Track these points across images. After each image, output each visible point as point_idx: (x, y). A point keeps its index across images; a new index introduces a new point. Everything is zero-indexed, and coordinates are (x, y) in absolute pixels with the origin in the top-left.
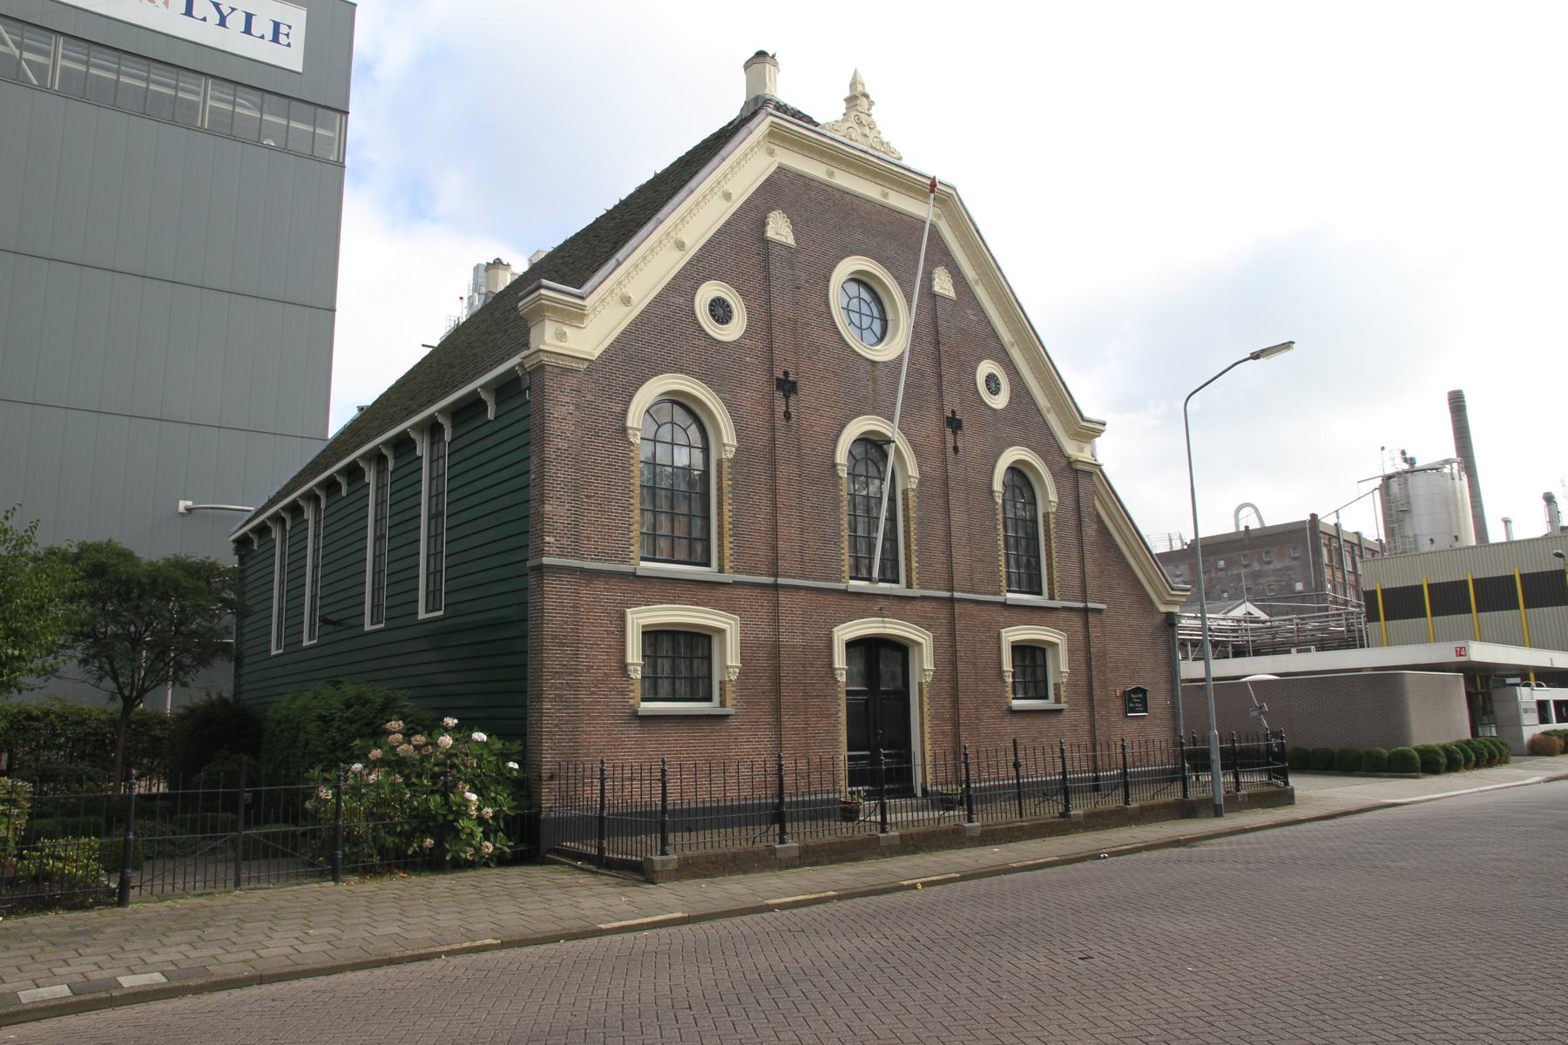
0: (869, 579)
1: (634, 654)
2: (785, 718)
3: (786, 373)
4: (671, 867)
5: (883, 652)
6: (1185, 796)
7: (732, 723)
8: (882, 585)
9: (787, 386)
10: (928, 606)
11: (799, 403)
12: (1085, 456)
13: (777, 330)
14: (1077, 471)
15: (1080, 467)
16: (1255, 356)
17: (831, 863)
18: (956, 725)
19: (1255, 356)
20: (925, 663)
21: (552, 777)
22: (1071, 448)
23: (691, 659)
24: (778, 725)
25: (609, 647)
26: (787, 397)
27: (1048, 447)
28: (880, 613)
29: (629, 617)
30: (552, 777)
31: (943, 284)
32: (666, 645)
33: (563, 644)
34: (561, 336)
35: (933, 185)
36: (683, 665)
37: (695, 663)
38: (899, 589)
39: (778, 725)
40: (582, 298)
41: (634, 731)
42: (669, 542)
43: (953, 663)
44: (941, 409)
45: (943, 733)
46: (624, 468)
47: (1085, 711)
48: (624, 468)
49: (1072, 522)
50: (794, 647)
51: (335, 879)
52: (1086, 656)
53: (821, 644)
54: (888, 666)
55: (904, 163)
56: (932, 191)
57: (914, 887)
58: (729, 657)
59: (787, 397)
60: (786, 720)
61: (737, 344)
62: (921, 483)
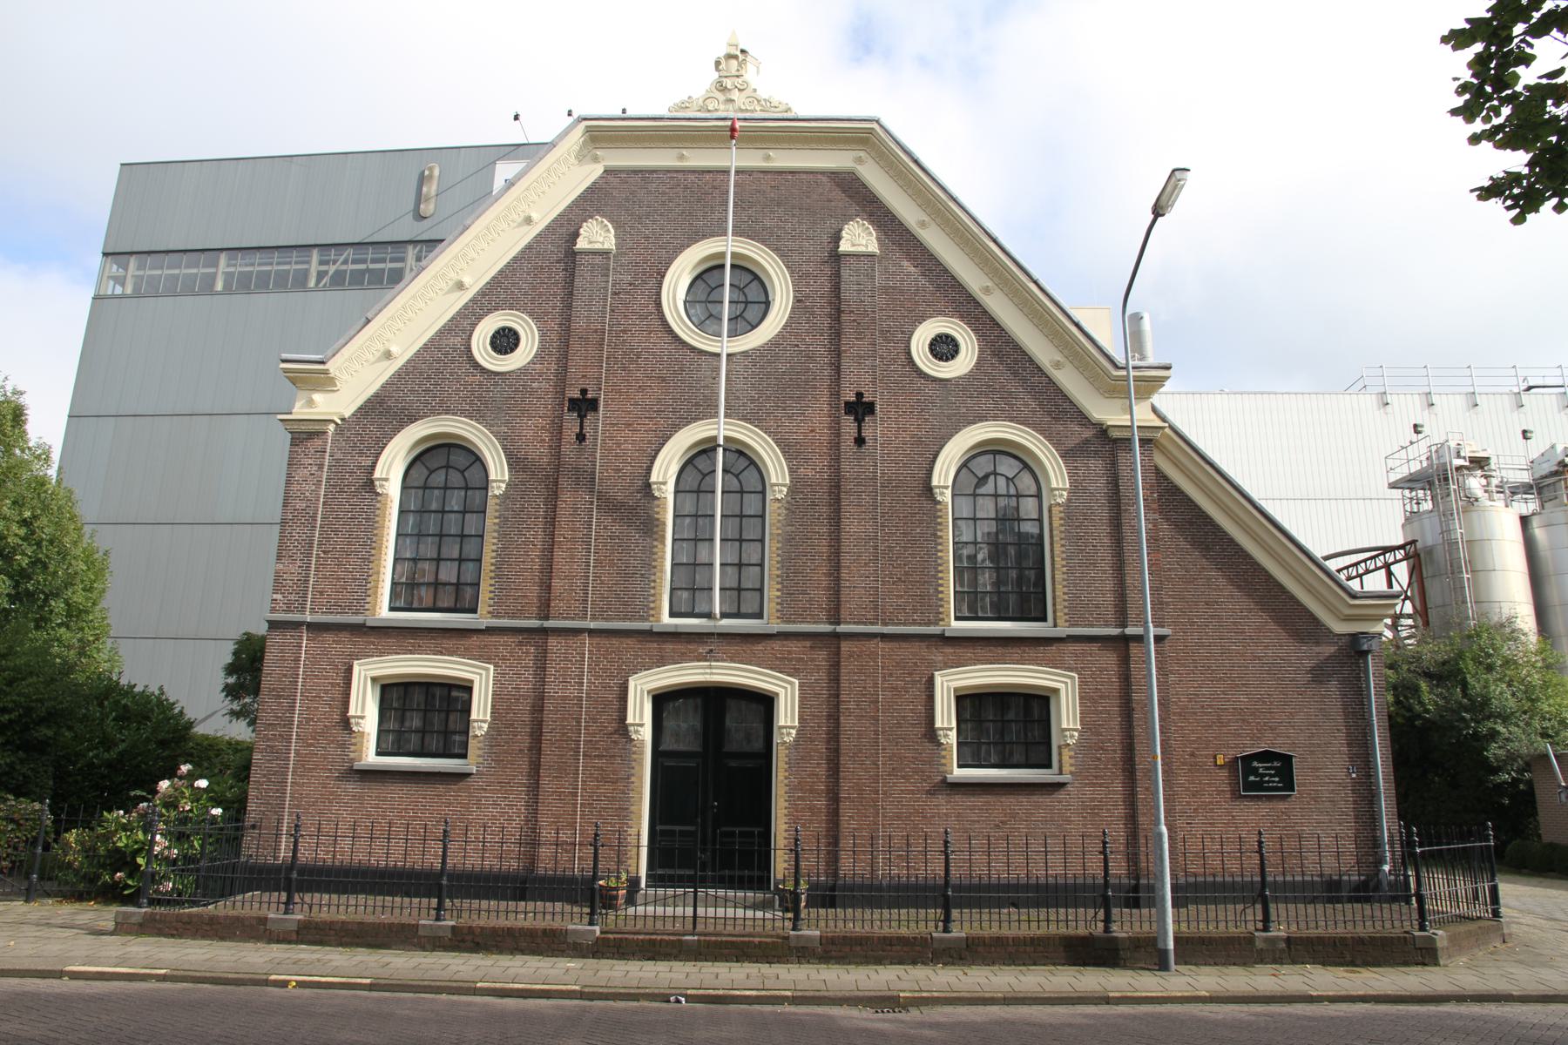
0: (709, 615)
1: (945, 717)
2: (544, 781)
3: (584, 392)
4: (133, 920)
5: (732, 704)
6: (1107, 929)
7: (1069, 788)
8: (725, 622)
9: (585, 405)
10: (794, 646)
11: (598, 424)
12: (1142, 415)
13: (575, 345)
14: (1116, 441)
15: (1115, 434)
16: (1158, 211)
17: (341, 945)
18: (834, 797)
19: (1158, 211)
20: (787, 716)
21: (254, 827)
22: (1110, 414)
23: (448, 712)
24: (534, 788)
25: (333, 699)
26: (582, 417)
27: (1055, 410)
28: (682, 658)
29: (356, 669)
30: (254, 827)
31: (859, 238)
32: (968, 702)
33: (279, 697)
34: (310, 403)
35: (733, 129)
36: (437, 719)
37: (452, 717)
38: (770, 623)
39: (534, 788)
40: (323, 363)
41: (352, 787)
42: (431, 590)
43: (834, 717)
44: (836, 394)
45: (811, 809)
46: (368, 520)
47: (1118, 786)
48: (368, 520)
49: (1102, 513)
50: (564, 698)
51: (27, 901)
52: (1121, 706)
53: (611, 696)
54: (736, 722)
55: (802, 113)
56: (732, 137)
57: (285, 984)
58: (1067, 718)
59: (582, 417)
60: (546, 782)
61: (523, 371)
62: (793, 490)
